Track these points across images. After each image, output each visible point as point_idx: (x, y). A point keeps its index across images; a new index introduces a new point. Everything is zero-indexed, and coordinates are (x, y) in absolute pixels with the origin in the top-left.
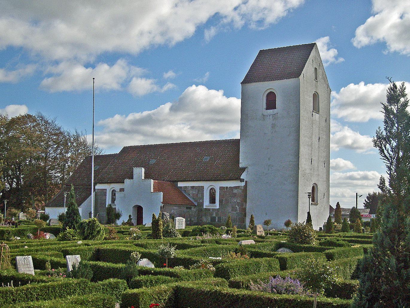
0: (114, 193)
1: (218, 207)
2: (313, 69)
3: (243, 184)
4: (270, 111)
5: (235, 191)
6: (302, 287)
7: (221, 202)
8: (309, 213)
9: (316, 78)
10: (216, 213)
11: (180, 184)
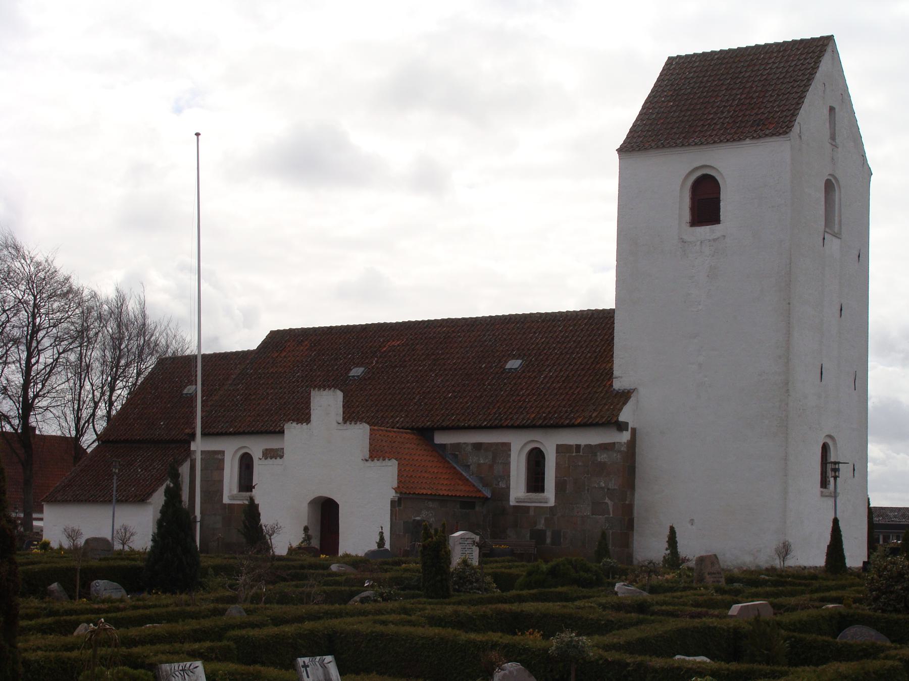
0: (246, 463)
1: (552, 502)
2: (826, 111)
3: (625, 437)
4: (704, 231)
5: (602, 457)
6: (168, 465)
7: (560, 486)
8: (836, 522)
9: (833, 137)
10: (546, 519)
11: (441, 439)
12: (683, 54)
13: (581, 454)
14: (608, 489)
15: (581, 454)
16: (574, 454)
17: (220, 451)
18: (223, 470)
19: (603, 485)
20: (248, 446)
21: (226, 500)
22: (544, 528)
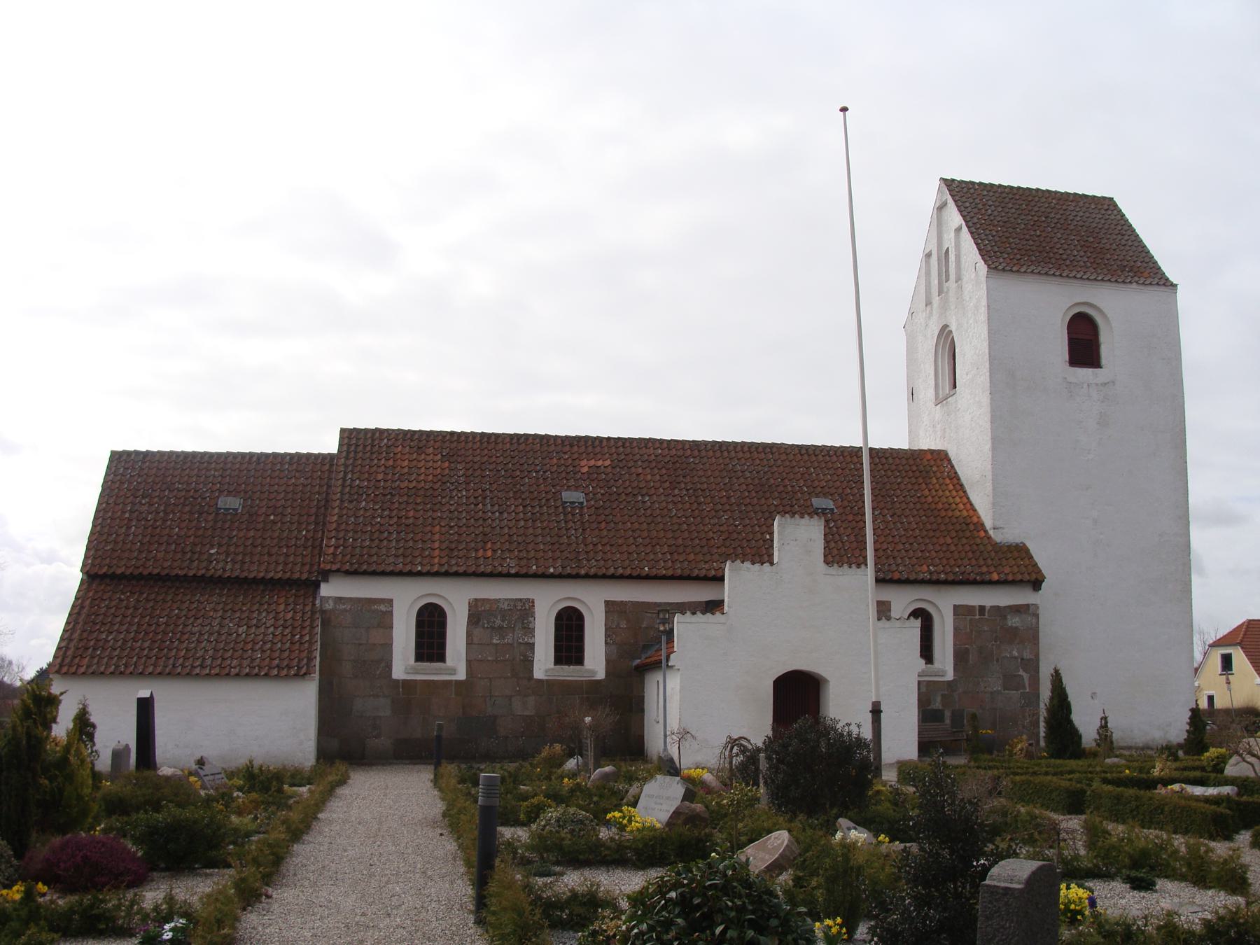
1: (950, 676)
7: (960, 657)
10: (943, 696)
12: (986, 182)
13: (986, 617)
14: (1022, 659)
15: (986, 617)
16: (977, 617)
17: (382, 599)
18: (392, 627)
19: (1016, 654)
20: (579, 597)
21: (398, 672)
22: (941, 708)
